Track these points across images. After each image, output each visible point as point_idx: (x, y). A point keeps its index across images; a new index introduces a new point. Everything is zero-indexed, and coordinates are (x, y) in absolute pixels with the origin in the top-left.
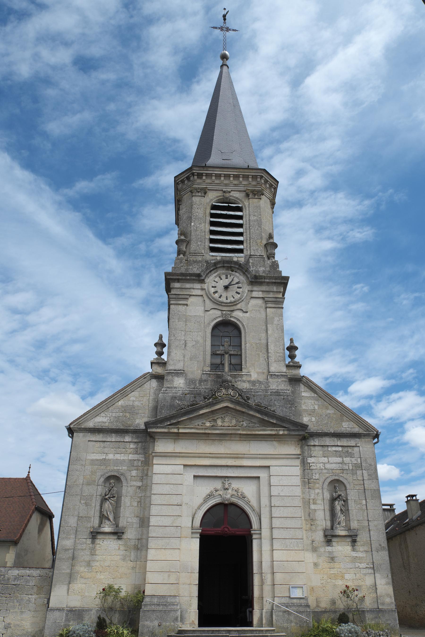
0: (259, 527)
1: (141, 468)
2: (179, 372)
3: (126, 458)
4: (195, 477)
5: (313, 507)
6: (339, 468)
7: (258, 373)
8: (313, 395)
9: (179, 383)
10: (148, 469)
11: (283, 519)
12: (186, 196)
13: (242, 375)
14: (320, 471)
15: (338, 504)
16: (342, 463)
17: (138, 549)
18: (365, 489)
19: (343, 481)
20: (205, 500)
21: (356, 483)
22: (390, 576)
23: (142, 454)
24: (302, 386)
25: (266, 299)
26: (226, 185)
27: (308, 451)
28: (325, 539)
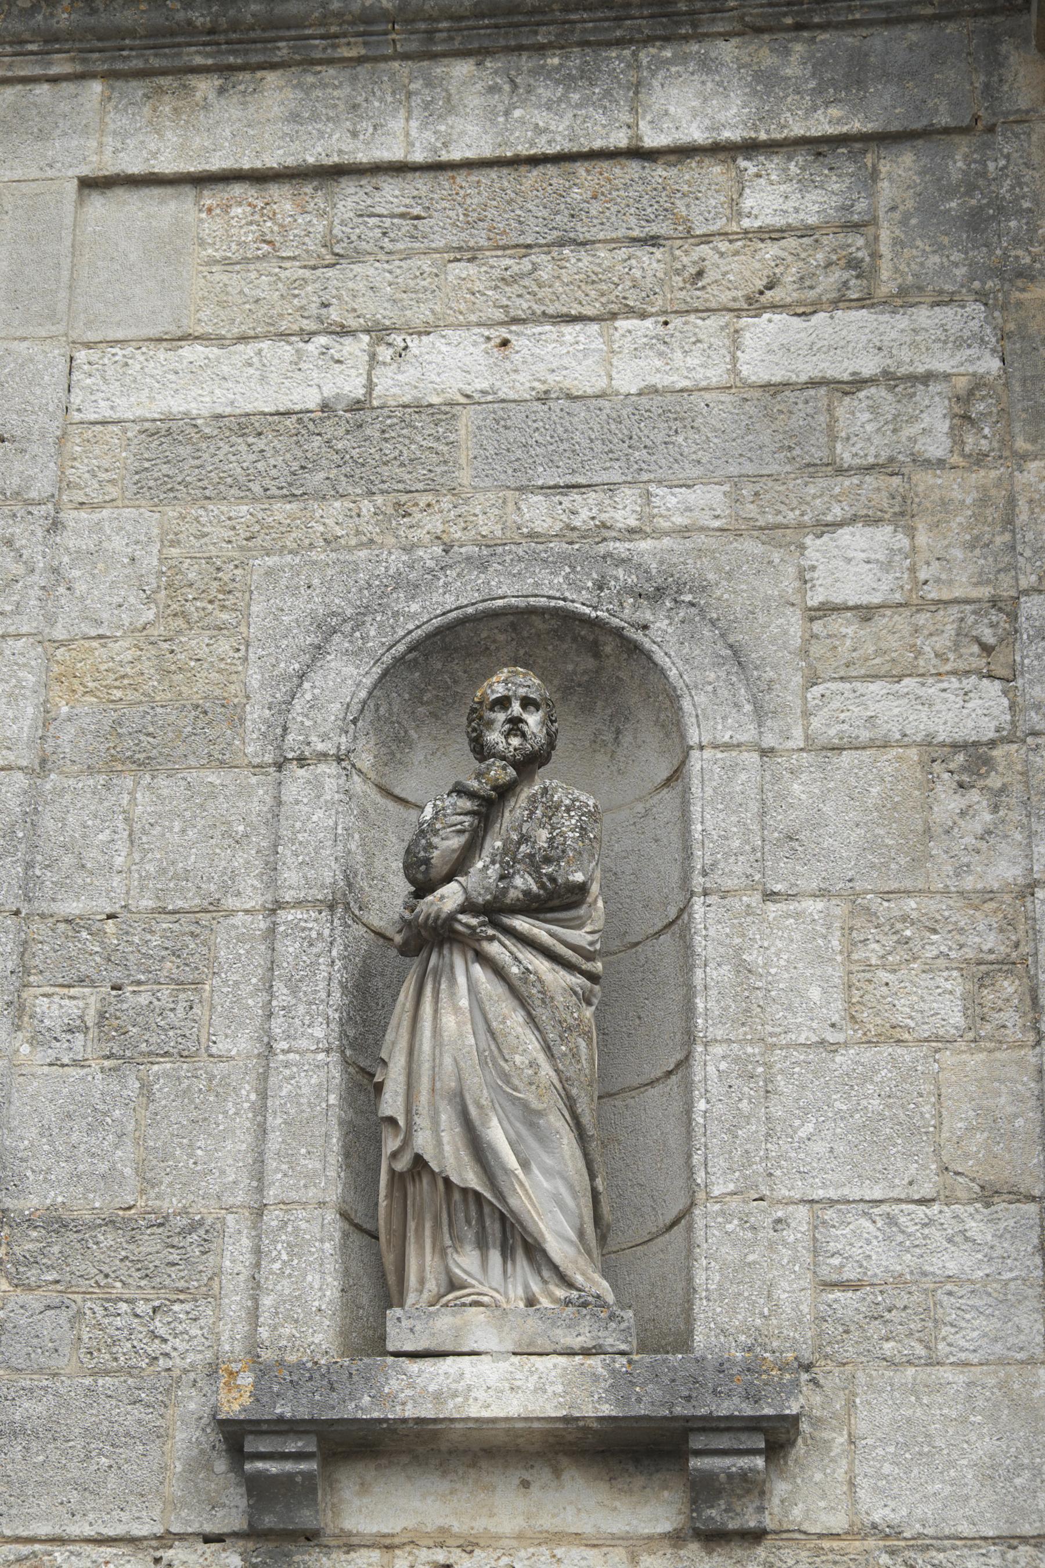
1: (961, 488)
3: (693, 360)
23: (943, 300)
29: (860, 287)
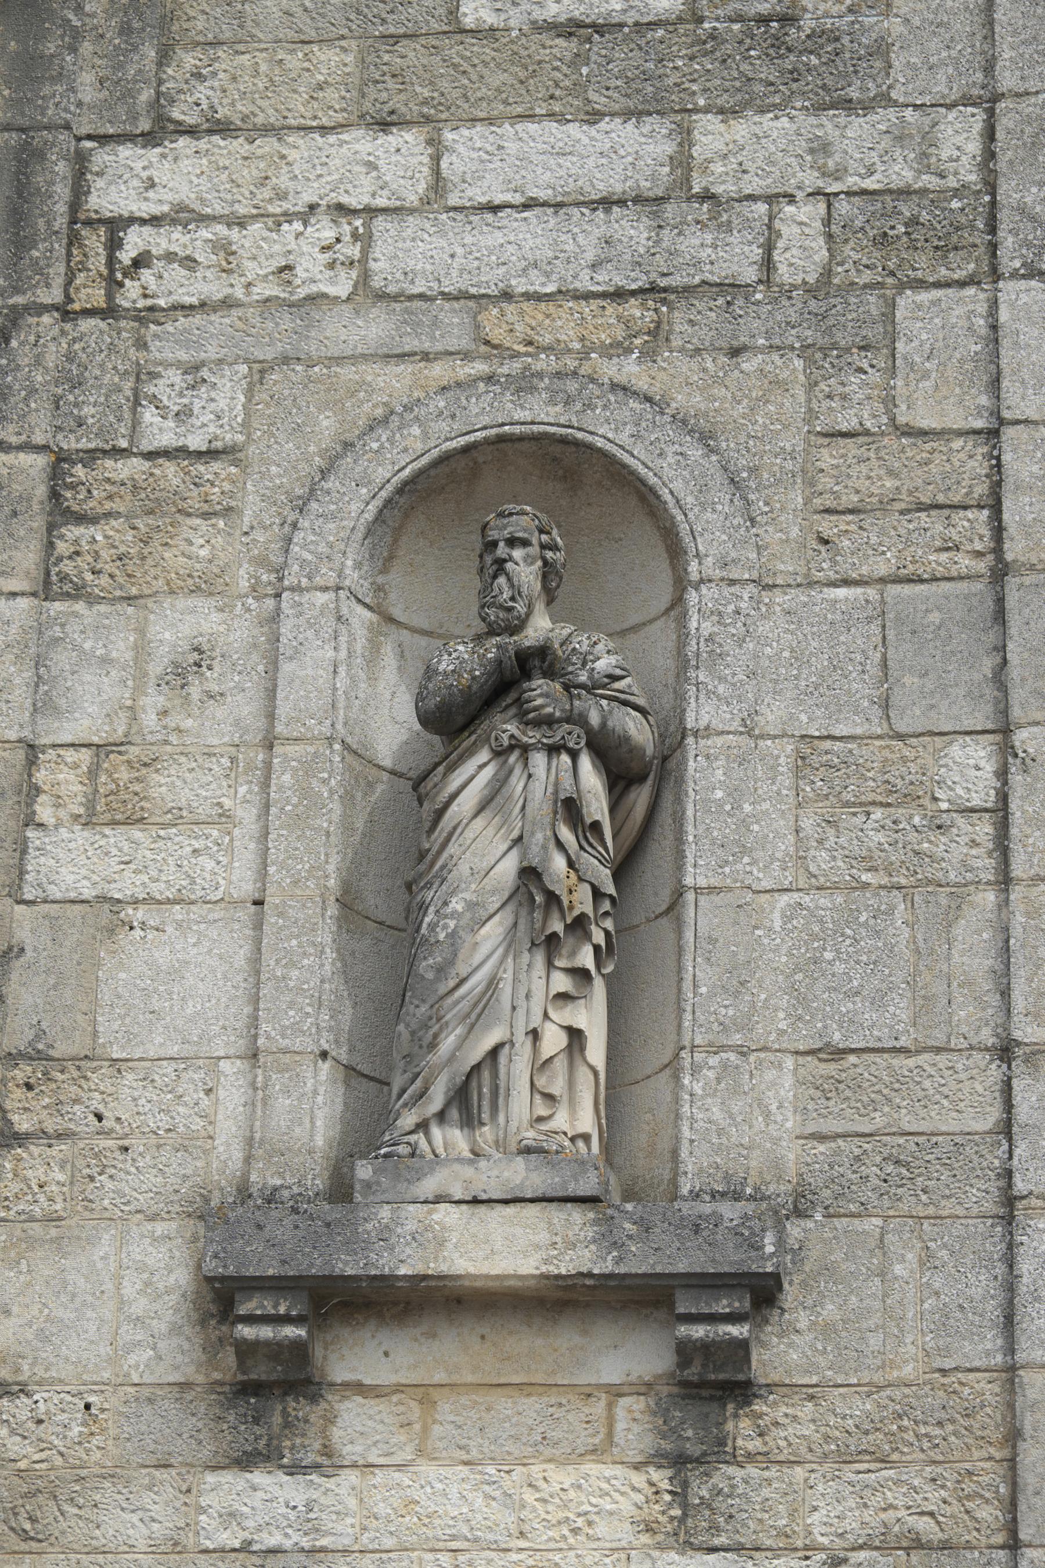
6: (607, 279)
14: (278, 334)
16: (679, 193)
18: (1001, 572)
19: (638, 458)
21: (859, 475)
27: (118, 59)
28: (212, 1349)
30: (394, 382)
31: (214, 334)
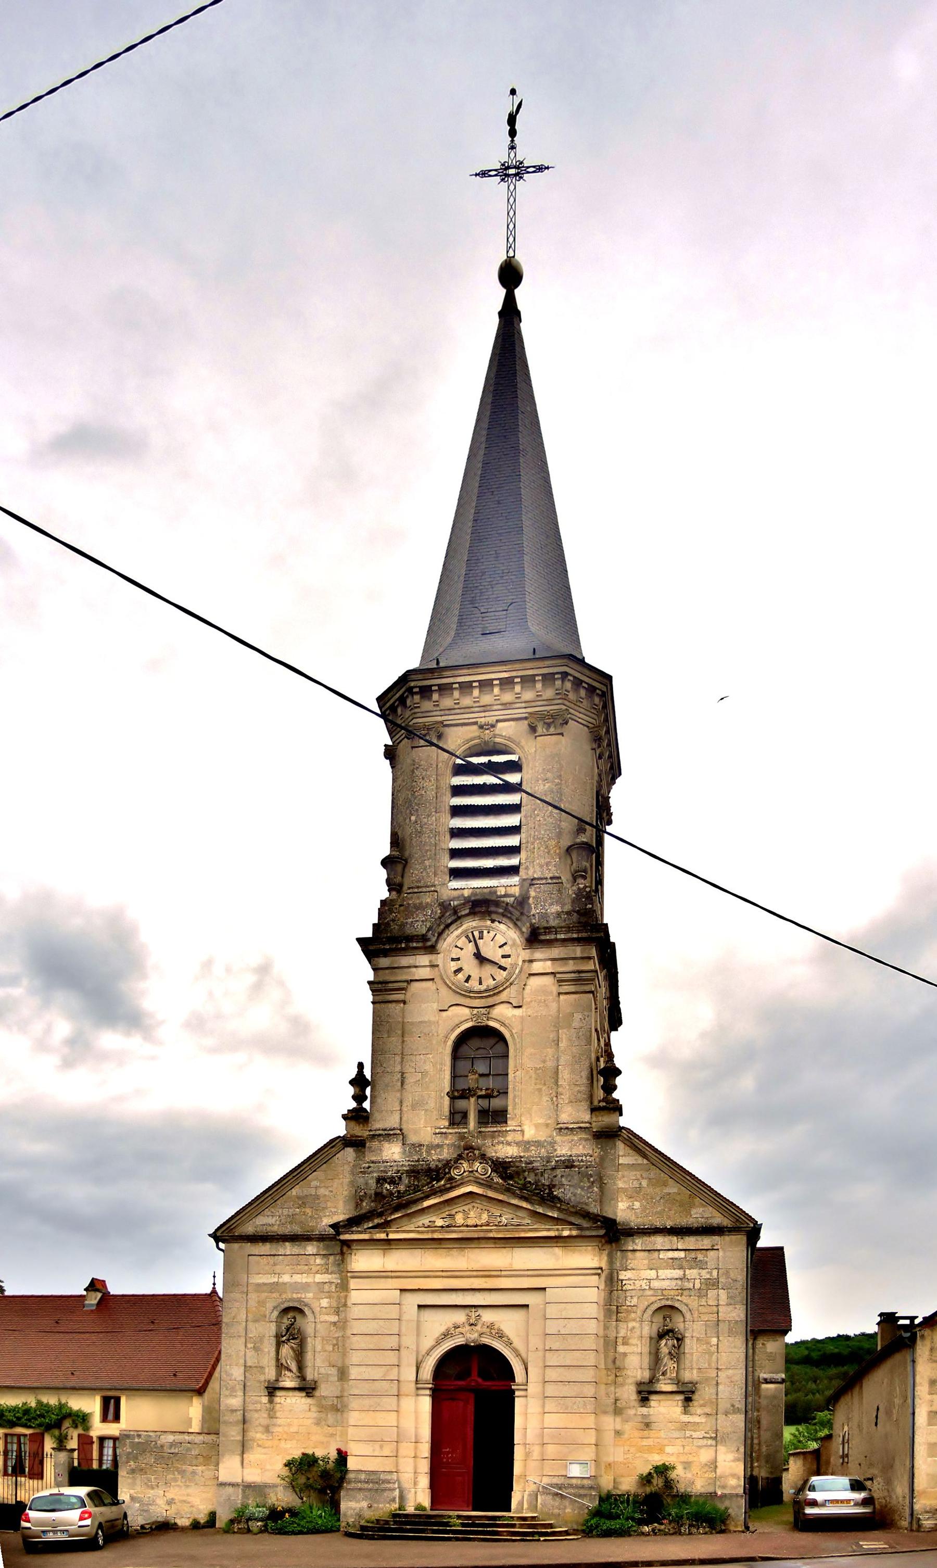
0: (525, 1381)
1: (335, 1295)
2: (391, 1132)
4: (419, 1306)
5: (621, 1349)
7: (537, 1126)
8: (641, 1160)
9: (393, 1152)
10: (346, 1296)
11: (562, 1369)
12: (401, 744)
13: (506, 1131)
15: (666, 1345)
16: (683, 1278)
17: (338, 1410)
20: (438, 1343)
22: (742, 1450)
24: (620, 1145)
25: (558, 976)
26: (486, 708)
29: (327, 1272)
30: (653, 1299)
31: (633, 1293)
